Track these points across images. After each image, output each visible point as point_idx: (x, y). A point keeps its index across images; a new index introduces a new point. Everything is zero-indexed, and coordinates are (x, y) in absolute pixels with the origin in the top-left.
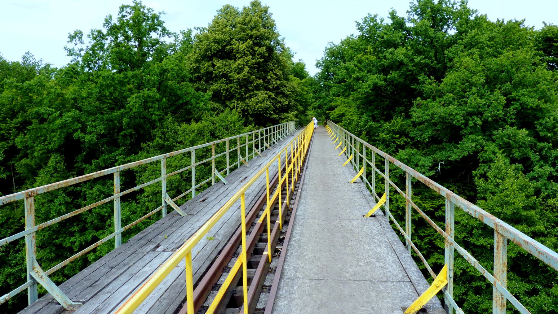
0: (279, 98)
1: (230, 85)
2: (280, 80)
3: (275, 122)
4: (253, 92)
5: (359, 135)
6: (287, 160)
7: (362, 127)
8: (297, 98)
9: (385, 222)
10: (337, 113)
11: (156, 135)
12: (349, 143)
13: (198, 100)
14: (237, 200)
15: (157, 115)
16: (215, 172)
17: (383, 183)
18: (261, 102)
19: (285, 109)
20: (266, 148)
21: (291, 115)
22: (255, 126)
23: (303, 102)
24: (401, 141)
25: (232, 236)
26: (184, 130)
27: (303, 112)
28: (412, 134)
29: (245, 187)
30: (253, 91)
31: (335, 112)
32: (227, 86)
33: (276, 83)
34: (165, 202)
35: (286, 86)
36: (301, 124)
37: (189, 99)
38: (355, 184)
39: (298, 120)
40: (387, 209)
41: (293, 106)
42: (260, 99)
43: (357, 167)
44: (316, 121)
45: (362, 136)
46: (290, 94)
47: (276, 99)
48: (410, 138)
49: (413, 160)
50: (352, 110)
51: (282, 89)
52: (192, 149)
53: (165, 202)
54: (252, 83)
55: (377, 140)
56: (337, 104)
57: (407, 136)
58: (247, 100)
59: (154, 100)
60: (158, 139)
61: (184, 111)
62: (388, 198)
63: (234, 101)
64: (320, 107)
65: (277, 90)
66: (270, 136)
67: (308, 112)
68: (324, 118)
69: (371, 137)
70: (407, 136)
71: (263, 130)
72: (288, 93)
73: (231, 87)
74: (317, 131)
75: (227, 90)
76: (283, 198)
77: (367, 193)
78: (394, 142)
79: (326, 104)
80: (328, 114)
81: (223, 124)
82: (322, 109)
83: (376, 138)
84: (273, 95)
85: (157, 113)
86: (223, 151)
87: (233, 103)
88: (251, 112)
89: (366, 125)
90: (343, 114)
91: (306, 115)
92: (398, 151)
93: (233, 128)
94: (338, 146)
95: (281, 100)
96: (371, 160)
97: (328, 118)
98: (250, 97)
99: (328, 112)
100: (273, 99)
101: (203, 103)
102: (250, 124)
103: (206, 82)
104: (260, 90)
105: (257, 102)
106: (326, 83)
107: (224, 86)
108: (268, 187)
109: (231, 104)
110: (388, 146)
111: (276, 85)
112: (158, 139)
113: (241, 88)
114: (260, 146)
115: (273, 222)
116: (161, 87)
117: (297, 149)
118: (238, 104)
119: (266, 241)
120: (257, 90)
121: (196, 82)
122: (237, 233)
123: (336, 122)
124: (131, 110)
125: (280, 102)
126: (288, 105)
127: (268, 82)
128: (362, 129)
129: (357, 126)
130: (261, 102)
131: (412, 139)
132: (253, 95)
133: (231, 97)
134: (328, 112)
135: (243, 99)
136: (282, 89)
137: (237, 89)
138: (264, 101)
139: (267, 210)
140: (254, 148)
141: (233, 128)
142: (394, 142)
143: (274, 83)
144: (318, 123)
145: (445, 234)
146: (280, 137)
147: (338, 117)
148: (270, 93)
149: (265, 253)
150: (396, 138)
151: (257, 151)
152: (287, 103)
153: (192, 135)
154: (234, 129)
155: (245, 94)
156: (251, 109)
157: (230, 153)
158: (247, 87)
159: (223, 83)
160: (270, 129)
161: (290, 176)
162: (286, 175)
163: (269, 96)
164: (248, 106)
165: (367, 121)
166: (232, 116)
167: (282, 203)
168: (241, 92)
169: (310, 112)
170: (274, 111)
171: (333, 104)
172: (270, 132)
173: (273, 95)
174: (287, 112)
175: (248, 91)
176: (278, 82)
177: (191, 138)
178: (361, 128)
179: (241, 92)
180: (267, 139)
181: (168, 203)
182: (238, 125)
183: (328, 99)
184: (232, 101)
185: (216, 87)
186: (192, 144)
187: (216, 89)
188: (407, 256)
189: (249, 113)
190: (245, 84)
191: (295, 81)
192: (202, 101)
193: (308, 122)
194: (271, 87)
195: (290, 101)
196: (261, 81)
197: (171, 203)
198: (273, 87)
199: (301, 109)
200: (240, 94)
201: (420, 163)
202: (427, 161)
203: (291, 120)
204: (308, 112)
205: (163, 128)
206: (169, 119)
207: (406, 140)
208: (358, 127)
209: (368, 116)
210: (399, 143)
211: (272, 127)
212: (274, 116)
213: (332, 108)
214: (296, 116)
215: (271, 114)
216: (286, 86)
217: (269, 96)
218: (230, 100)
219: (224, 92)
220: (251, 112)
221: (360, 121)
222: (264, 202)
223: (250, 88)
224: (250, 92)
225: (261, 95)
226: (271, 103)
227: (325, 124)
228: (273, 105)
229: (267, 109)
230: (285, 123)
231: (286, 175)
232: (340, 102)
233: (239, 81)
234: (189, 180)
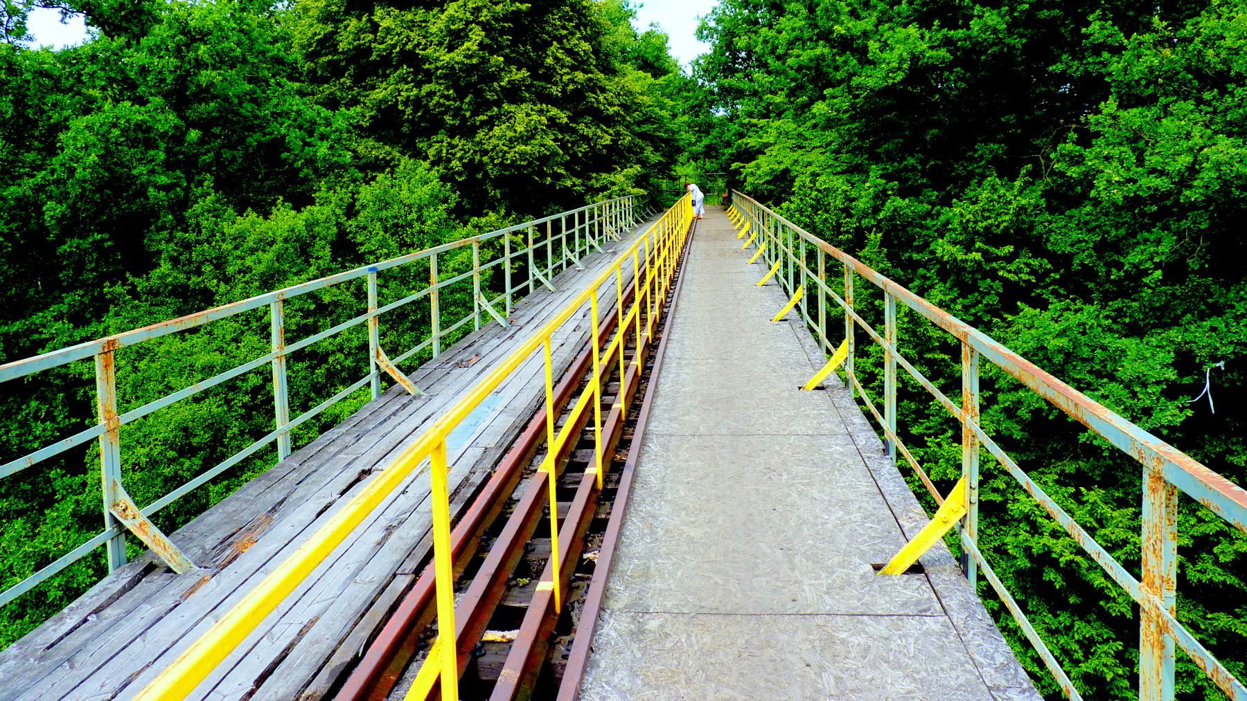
0: (582, 126)
1: (426, 88)
2: (585, 72)
3: (571, 200)
4: (499, 107)
5: (854, 246)
6: (648, 260)
7: (865, 215)
8: (646, 128)
9: (847, 400)
10: (765, 168)
11: (160, 252)
12: (790, 252)
13: (311, 134)
14: (643, 240)
15: (167, 188)
16: (480, 300)
17: (957, 438)
18: (526, 138)
19: (607, 160)
20: (569, 263)
21: (620, 177)
22: (508, 214)
23: (662, 139)
24: (1021, 268)
25: (532, 417)
26: (240, 238)
27: (664, 169)
28: (1059, 243)
29: (476, 395)
30: (498, 103)
31: (758, 167)
32: (415, 91)
33: (572, 81)
34: (378, 367)
35: (603, 90)
36: (654, 204)
37: (283, 131)
38: (821, 392)
39: (642, 191)
40: (970, 542)
41: (630, 150)
42: (519, 133)
43: (790, 288)
44: (700, 195)
45: (865, 252)
46: (618, 114)
47: (574, 131)
48: (1052, 257)
49: (1085, 352)
50: (818, 158)
51: (591, 97)
52: (272, 302)
53: (378, 367)
54: (495, 77)
55: (919, 264)
56: (765, 140)
57: (1037, 247)
58: (480, 135)
59: (142, 136)
60: (165, 267)
61: (265, 175)
62: (975, 499)
63: (440, 137)
64: (710, 152)
65: (575, 100)
66: (582, 231)
67: (679, 170)
68: (721, 183)
69: (903, 251)
70: (1037, 247)
71: (529, 225)
72: (612, 110)
73: (431, 94)
74: (701, 228)
75: (417, 103)
76: (628, 358)
77: (866, 435)
78: (993, 274)
79: (728, 144)
80: (737, 172)
81: (384, 214)
82: (716, 157)
83: (915, 256)
84: (563, 117)
85: (163, 180)
86: (358, 314)
87: (438, 144)
88: (493, 172)
89: (876, 210)
90: (786, 171)
91: (674, 179)
92: (1016, 311)
93: (417, 226)
94: (757, 255)
95: (589, 132)
96: (815, 272)
97: (735, 182)
98: (490, 124)
99: (734, 166)
100: (564, 129)
101: (326, 144)
102: (494, 209)
103: (358, 79)
104: (523, 100)
105: (510, 140)
106: (726, 82)
107: (409, 91)
108: (596, 335)
109: (430, 146)
110: (966, 289)
111: (571, 87)
112: (165, 267)
113: (461, 96)
114: (512, 281)
115: (606, 407)
116: (180, 95)
117: (652, 262)
118: (453, 147)
119: (592, 445)
120: (511, 102)
121: (326, 80)
122: (588, 347)
123: (761, 198)
124: (72, 171)
125: (585, 139)
126: (613, 147)
127: (549, 76)
128: (865, 222)
129: (847, 211)
130: (526, 138)
131: (1061, 261)
132: (498, 117)
133: (430, 124)
134: (734, 166)
135: (466, 131)
136: (591, 97)
137: (447, 98)
138: (533, 137)
139: (547, 466)
140: (533, 269)
141: (417, 226)
142: (993, 274)
143: (565, 78)
144: (705, 200)
145: (856, 317)
146: (623, 224)
147: (768, 182)
148: (554, 111)
149: (588, 471)
150: (998, 258)
151: (570, 256)
152: (607, 140)
153: (268, 256)
154: (421, 232)
155: (475, 113)
156: (492, 159)
157: (535, 251)
158: (479, 94)
159: (403, 80)
160: (582, 215)
161: (643, 310)
162: (647, 286)
163: (552, 120)
164: (485, 152)
165: (881, 196)
166: (417, 183)
167: (626, 368)
168: (460, 108)
169: (685, 170)
170: (567, 165)
171: (752, 141)
172: (582, 221)
173: (563, 117)
174: (610, 170)
175: (481, 105)
176: (580, 76)
177: (261, 268)
178: (859, 220)
179: (460, 108)
180: (570, 238)
181: (383, 368)
182: (437, 213)
183: (734, 127)
184: (434, 138)
185: (381, 96)
186: (268, 282)
187: (384, 101)
188: (889, 468)
189: (486, 174)
190: (470, 81)
191: (635, 80)
192: (323, 137)
193: (680, 193)
194: (555, 91)
195: (618, 134)
196: (524, 73)
197: (138, 520)
198: (564, 91)
199: (655, 158)
200: (457, 113)
201: (1128, 369)
202: (1148, 358)
203: (622, 192)
204: (679, 170)
205: (186, 231)
206: (206, 200)
207: (1035, 263)
208: (850, 215)
209: (888, 177)
210: (1011, 277)
211: (563, 215)
212: (569, 183)
213: (748, 155)
214: (640, 181)
215: (558, 177)
216: (603, 90)
217: (552, 120)
218: (428, 133)
219: (409, 110)
220: (493, 172)
221: (853, 194)
222: (586, 367)
223: (490, 96)
224: (490, 109)
225: (524, 116)
226: (555, 140)
227: (727, 203)
228: (563, 146)
229: (544, 159)
230: (601, 200)
231: (647, 286)
232: (775, 133)
233: (451, 75)
234: (261, 404)
